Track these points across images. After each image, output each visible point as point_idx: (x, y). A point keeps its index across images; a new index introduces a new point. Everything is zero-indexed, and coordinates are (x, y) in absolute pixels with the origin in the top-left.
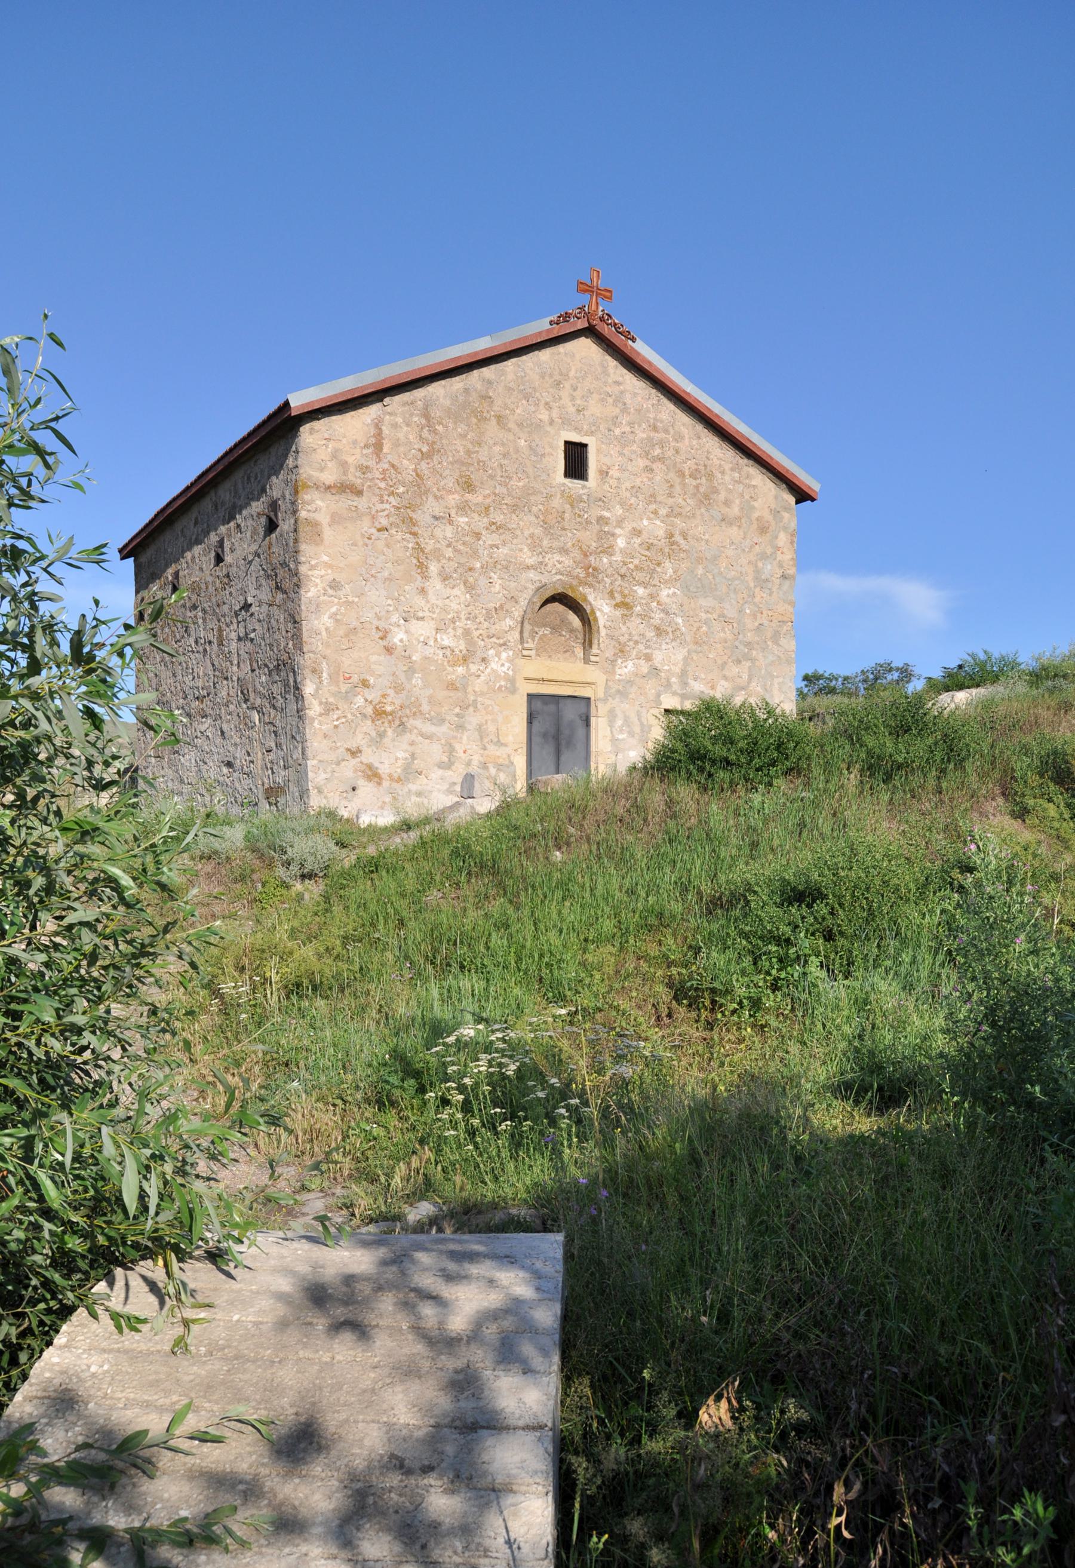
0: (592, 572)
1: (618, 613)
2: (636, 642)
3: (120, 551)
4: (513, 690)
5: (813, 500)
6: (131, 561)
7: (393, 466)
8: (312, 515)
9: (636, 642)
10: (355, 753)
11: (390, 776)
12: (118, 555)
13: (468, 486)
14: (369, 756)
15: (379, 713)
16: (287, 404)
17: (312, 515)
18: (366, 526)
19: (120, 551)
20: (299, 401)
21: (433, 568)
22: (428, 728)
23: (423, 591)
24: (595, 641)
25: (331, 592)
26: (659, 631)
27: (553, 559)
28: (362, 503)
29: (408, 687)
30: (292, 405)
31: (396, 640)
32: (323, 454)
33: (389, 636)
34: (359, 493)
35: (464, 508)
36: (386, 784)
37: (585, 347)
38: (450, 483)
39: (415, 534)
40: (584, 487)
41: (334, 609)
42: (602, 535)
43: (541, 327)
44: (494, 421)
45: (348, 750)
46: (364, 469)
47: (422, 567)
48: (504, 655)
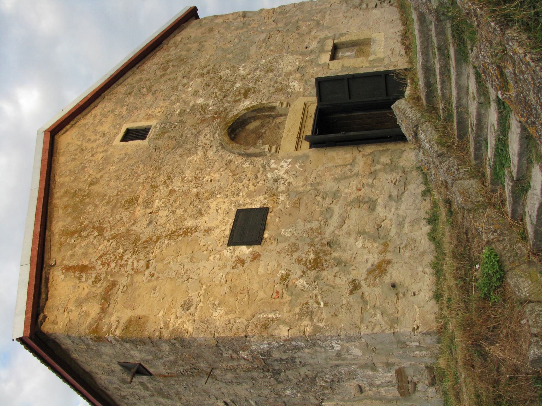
2: (276, 82)
7: (101, 257)
10: (355, 286)
11: (381, 252)
14: (360, 273)
21: (190, 223)
23: (208, 231)
25: (192, 309)
26: (270, 70)
28: (123, 281)
29: (293, 240)
34: (114, 284)
35: (148, 204)
36: (389, 256)
38: (126, 215)
44: (93, 187)
45: (351, 292)
47: (188, 232)
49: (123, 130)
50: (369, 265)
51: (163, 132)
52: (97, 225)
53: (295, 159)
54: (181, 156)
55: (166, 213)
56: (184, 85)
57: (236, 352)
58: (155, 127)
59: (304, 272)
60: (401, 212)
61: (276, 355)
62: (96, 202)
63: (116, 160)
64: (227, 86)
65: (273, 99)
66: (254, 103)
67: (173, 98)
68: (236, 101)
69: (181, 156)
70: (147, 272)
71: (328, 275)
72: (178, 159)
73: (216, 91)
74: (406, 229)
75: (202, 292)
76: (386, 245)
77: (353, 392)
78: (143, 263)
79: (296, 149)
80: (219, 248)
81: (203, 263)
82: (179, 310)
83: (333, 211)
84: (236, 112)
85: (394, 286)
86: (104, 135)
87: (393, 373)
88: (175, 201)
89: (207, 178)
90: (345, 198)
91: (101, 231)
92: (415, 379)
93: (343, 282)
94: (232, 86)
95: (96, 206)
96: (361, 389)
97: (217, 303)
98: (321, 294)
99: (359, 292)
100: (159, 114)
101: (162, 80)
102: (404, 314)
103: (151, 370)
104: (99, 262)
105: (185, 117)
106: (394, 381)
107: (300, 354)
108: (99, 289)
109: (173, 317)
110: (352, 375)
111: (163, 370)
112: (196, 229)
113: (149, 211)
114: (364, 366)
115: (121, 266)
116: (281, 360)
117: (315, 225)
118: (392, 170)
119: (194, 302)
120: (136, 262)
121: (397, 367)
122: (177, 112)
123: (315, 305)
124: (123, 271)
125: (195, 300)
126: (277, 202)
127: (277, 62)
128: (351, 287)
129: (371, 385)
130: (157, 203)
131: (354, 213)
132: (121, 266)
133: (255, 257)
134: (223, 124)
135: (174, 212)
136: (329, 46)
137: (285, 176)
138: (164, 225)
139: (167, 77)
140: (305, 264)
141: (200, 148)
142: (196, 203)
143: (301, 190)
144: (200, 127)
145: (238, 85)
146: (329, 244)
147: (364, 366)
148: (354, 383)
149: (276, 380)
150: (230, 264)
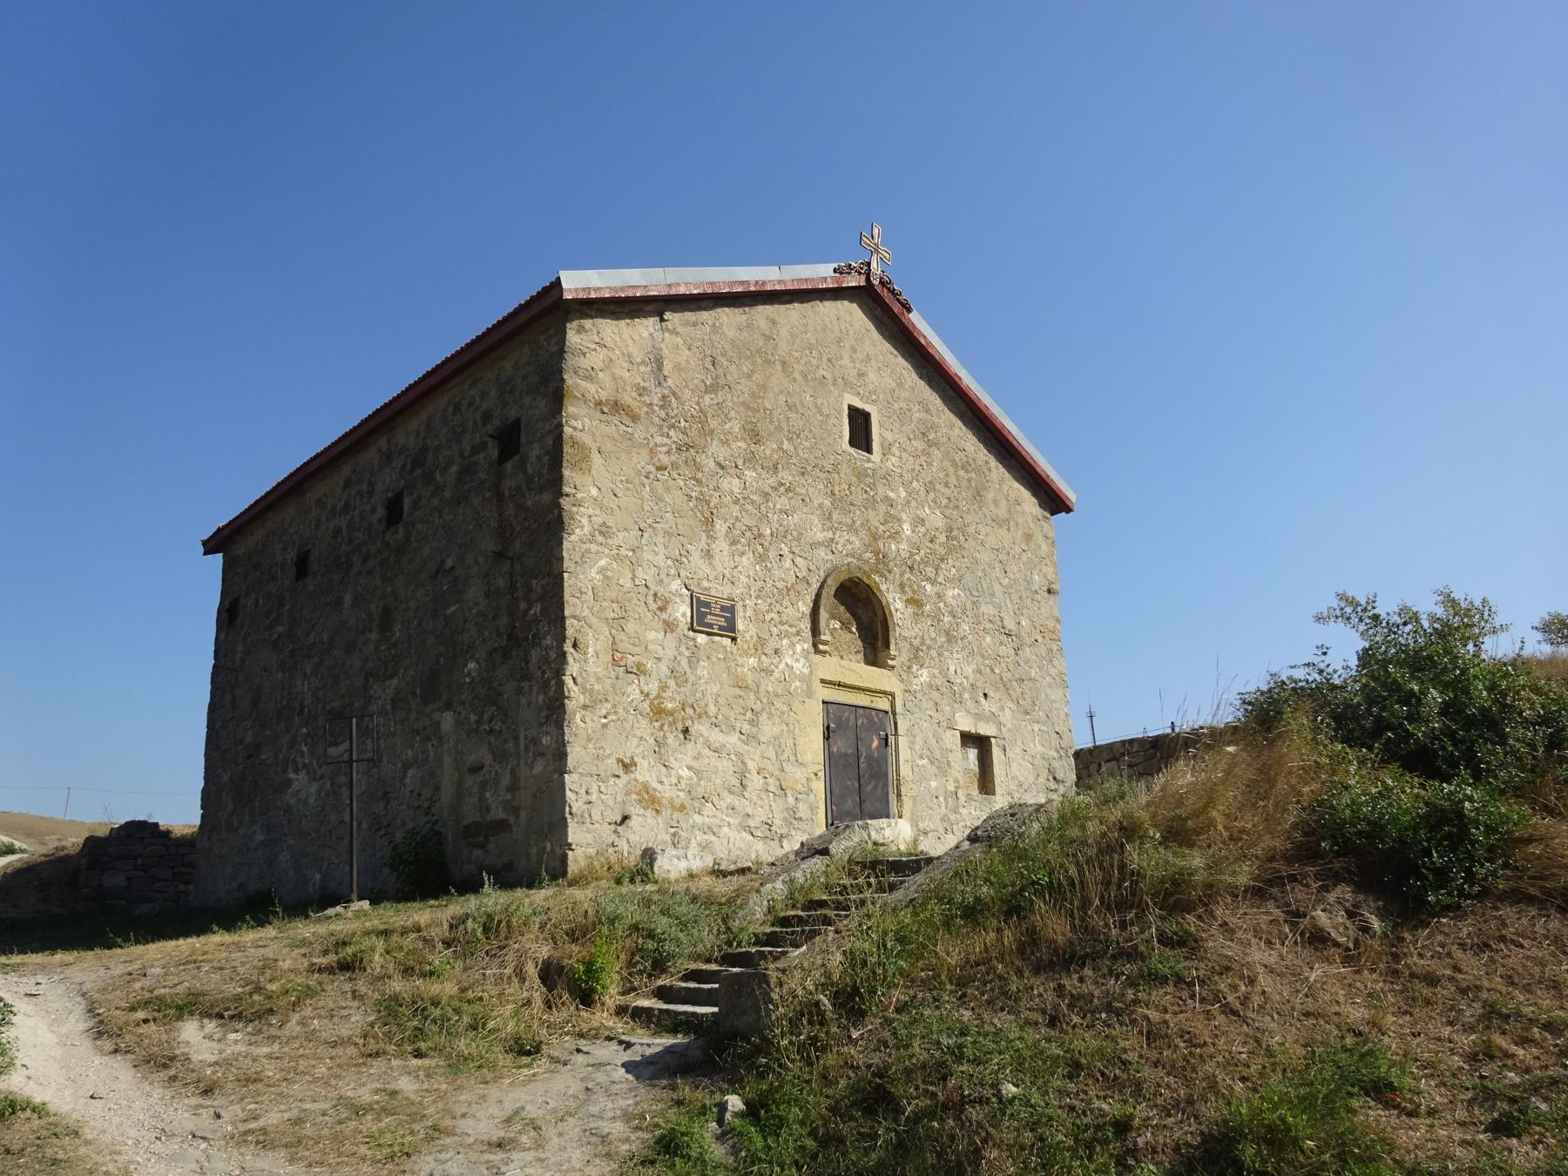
0: (882, 559)
1: (910, 610)
2: (929, 648)
3: (205, 543)
4: (810, 694)
5: (1068, 510)
6: (218, 558)
7: (674, 394)
8: (579, 434)
9: (929, 648)
10: (628, 766)
11: (671, 802)
12: (202, 549)
13: (755, 436)
14: (646, 773)
15: (658, 712)
16: (557, 284)
17: (579, 434)
18: (641, 460)
19: (205, 543)
20: (575, 283)
21: (720, 527)
22: (716, 737)
23: (708, 554)
24: (892, 641)
25: (600, 539)
26: (950, 639)
27: (842, 537)
28: (639, 431)
29: (692, 679)
30: (565, 285)
31: (678, 615)
32: (595, 359)
33: (669, 609)
34: (635, 418)
35: (751, 459)
36: (666, 813)
37: (851, 315)
38: (736, 427)
39: (699, 481)
40: (869, 460)
41: (602, 563)
42: (889, 518)
43: (821, 272)
44: (779, 367)
45: (620, 761)
46: (642, 391)
47: (709, 523)
48: (798, 648)
49: (867, 408)
50: (655, 785)
51: (861, 474)
52: (722, 381)
53: (806, 680)
54: (821, 506)
55: (736, 490)
56: (934, 501)
57: (541, 599)
58: (869, 460)
59: (647, 695)
60: (725, 829)
61: (535, 654)
62: (756, 376)
63: (819, 401)
64: (930, 571)
65: (901, 644)
66: (897, 616)
67: (915, 484)
68: (902, 586)
69: (821, 506)
70: (652, 468)
71: (645, 728)
72: (816, 502)
73: (922, 553)
74: (700, 837)
75: (623, 552)
76: (682, 808)
77: (472, 759)
78: (665, 460)
79: (823, 681)
80: (683, 573)
81: (661, 550)
82: (598, 520)
83: (728, 733)
84: (883, 587)
85: (625, 818)
86: (861, 375)
87: (501, 815)
88: (753, 502)
89: (786, 550)
90: (748, 752)
91: (712, 389)
92: (492, 846)
93: (631, 748)
94: (928, 579)
95: (749, 376)
96: (476, 769)
97: (609, 574)
98: (1283, 1159)
99: (620, 772)
100: (889, 464)
101: (946, 463)
102: (588, 831)
103: (509, 466)
104: (666, 392)
105: (882, 508)
106: (489, 819)
107: (535, 688)
108: (629, 398)
109: (591, 512)
110: (501, 756)
111: (508, 484)
112: (712, 538)
113: (740, 463)
114: (514, 776)
115: (661, 427)
116: (527, 662)
117: (712, 709)
118: (785, 819)
119: (610, 541)
120: (664, 449)
121: (512, 820)
122: (891, 494)
123: (604, 712)
124: (653, 430)
125: (613, 542)
126: (746, 654)
127: (963, 648)
128: (627, 761)
129: (483, 786)
130: (750, 474)
131: (725, 766)
132: (661, 427)
133: (669, 626)
134: (866, 568)
135: (736, 502)
136: (984, 730)
137: (782, 666)
138: (717, 488)
139: (951, 470)
140: (658, 696)
141: (830, 535)
142: (748, 534)
143: (762, 688)
144: (863, 533)
145: (929, 587)
146: (686, 731)
147: (514, 776)
148: (488, 759)
149: (495, 650)
150: (661, 590)
